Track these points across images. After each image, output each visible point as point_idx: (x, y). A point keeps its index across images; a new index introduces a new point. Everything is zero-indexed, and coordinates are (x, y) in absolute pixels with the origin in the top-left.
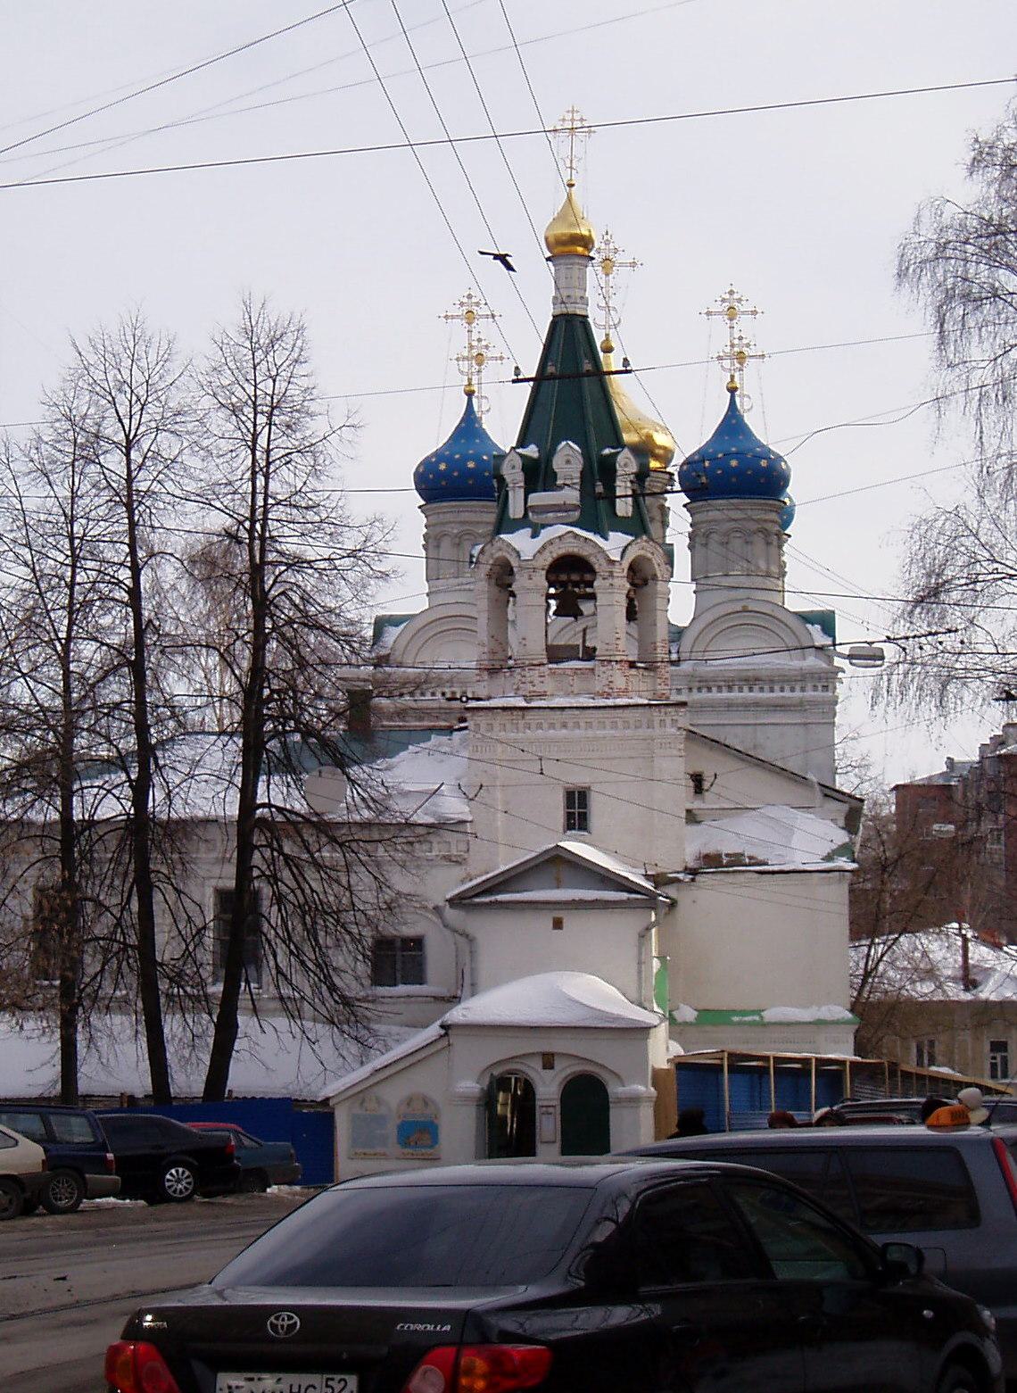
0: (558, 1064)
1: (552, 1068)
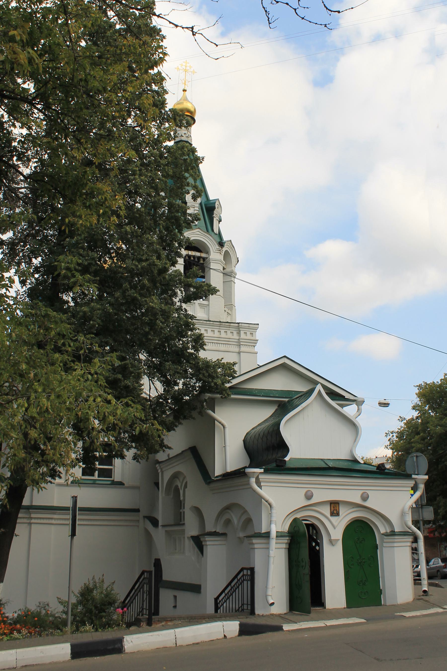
0: (342, 510)
1: (338, 514)
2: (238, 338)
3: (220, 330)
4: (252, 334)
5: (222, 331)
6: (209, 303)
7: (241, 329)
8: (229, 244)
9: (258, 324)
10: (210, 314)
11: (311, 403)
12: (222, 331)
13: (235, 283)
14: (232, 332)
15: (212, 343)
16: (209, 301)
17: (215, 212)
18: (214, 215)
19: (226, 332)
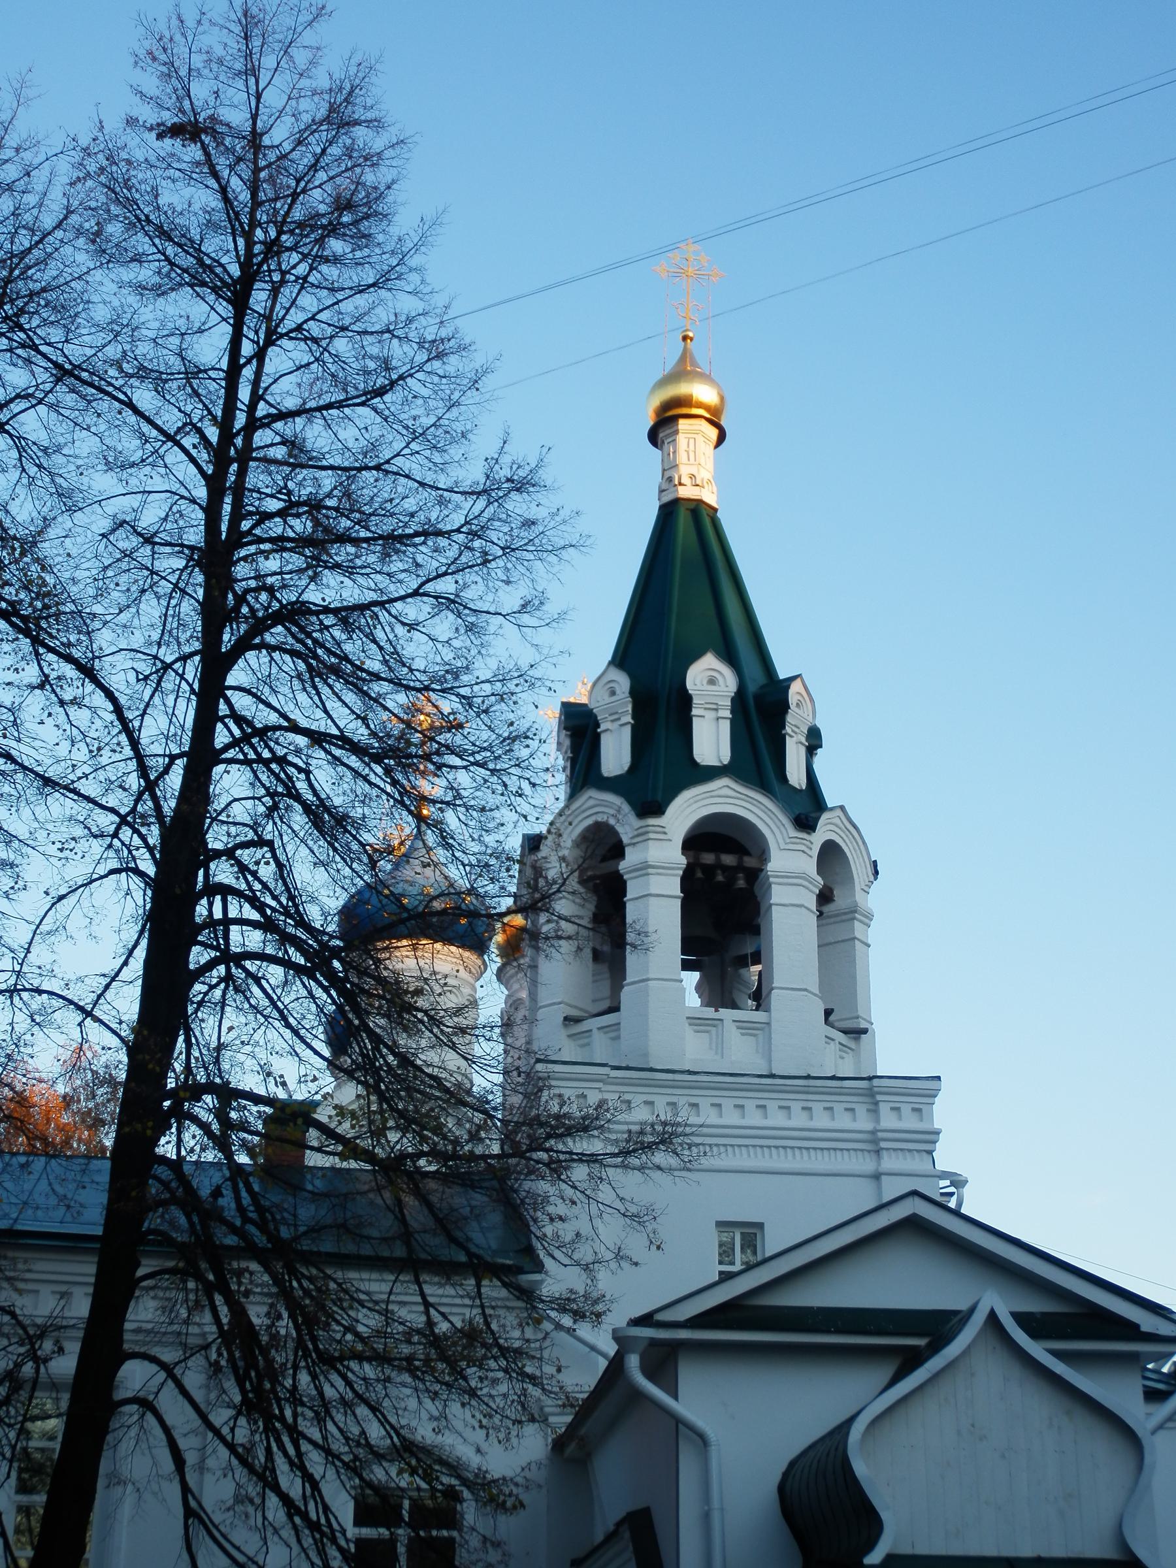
2: (869, 1126)
3: (809, 1104)
4: (918, 1110)
5: (836, 1106)
6: (770, 1017)
7: (879, 1098)
8: (837, 821)
9: (939, 1078)
10: (774, 1055)
11: (966, 1352)
12: (836, 1106)
13: (869, 946)
14: (852, 1110)
15: (784, 1148)
16: (768, 1010)
17: (790, 718)
18: (788, 730)
19: (831, 1109)
